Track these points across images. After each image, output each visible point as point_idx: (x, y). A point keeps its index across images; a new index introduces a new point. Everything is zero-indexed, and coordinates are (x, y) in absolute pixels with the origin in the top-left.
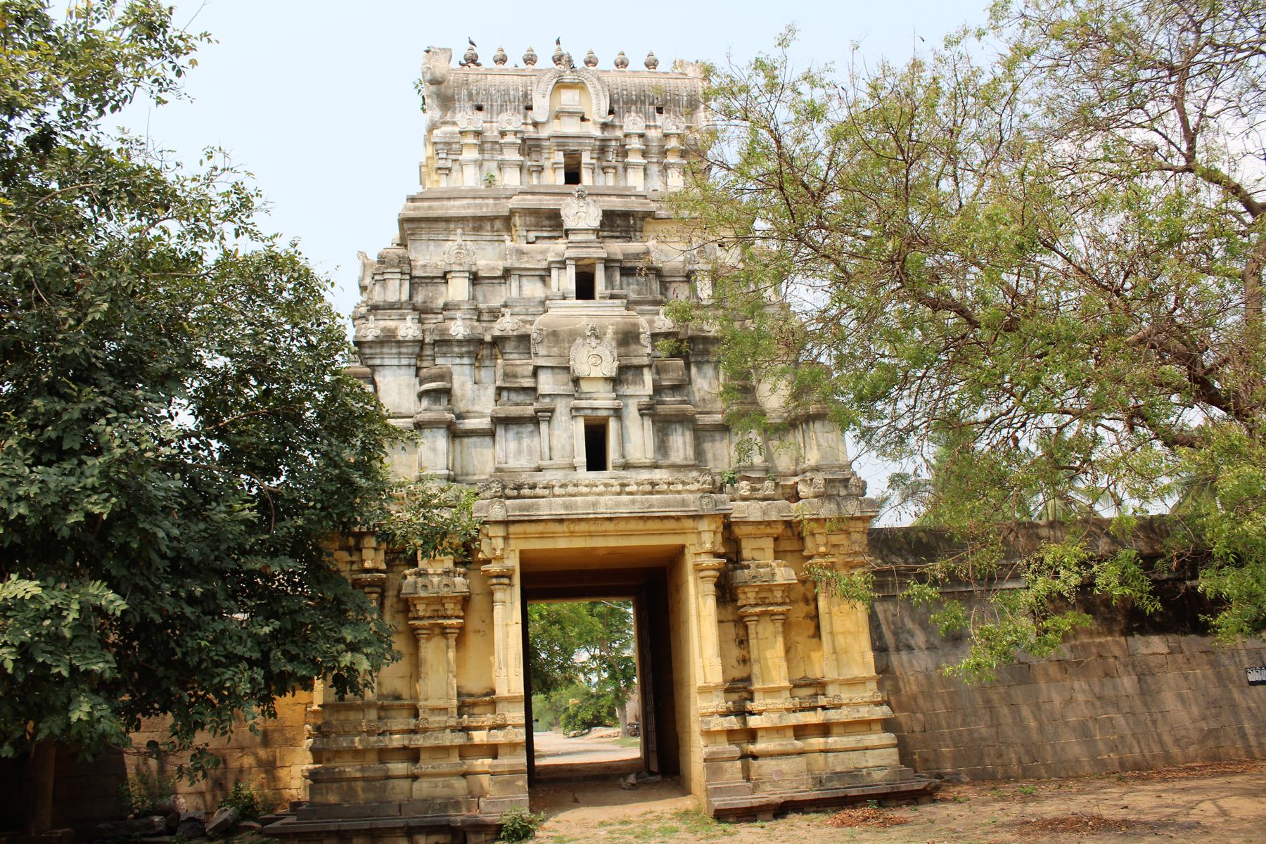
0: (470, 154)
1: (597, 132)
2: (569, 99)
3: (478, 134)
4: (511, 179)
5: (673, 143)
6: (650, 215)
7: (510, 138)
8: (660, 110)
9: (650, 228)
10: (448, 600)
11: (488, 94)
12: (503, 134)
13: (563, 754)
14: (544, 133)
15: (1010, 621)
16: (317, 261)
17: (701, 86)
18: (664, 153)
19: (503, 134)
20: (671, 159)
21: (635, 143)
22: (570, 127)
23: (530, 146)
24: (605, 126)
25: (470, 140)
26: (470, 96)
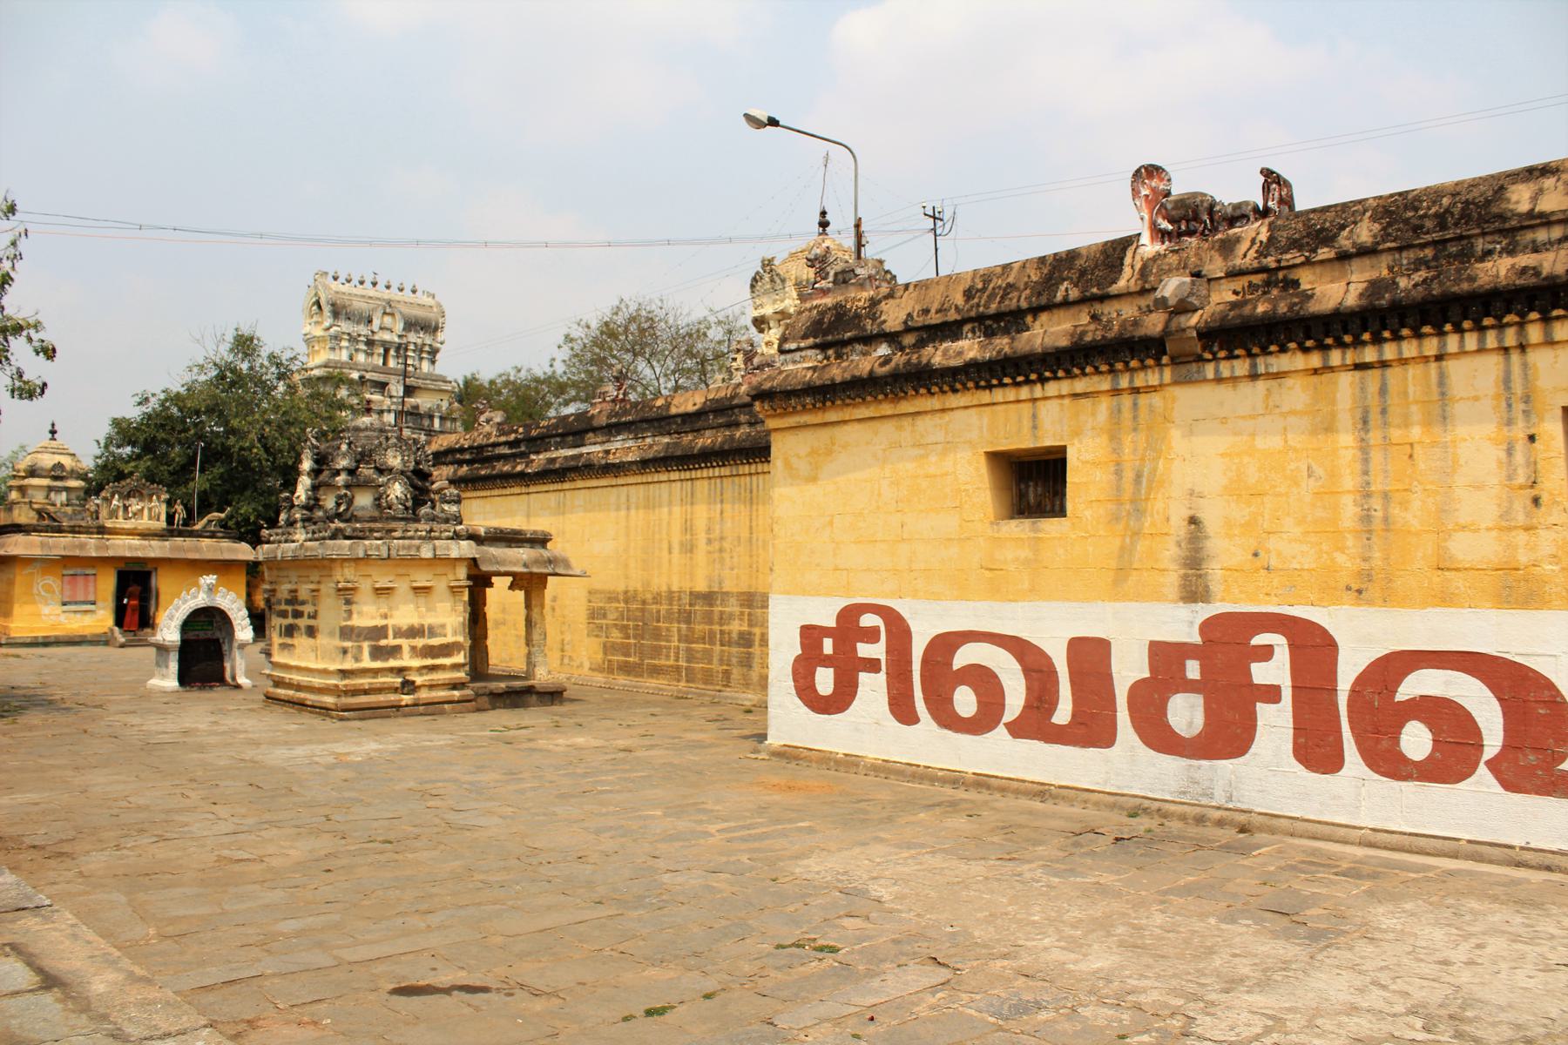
0: (344, 344)
1: (396, 339)
2: (388, 320)
3: (349, 334)
4: (361, 358)
5: (427, 348)
6: (419, 388)
7: (362, 338)
8: (422, 329)
9: (417, 392)
10: (367, 514)
11: (354, 314)
12: (359, 335)
13: (806, 426)
14: (376, 337)
15: (166, 442)
16: (934, 725)
17: (485, 442)
18: (422, 351)
19: (359, 335)
20: (424, 355)
21: (412, 347)
22: (387, 336)
23: (370, 343)
24: (400, 336)
25: (346, 337)
26: (346, 313)
